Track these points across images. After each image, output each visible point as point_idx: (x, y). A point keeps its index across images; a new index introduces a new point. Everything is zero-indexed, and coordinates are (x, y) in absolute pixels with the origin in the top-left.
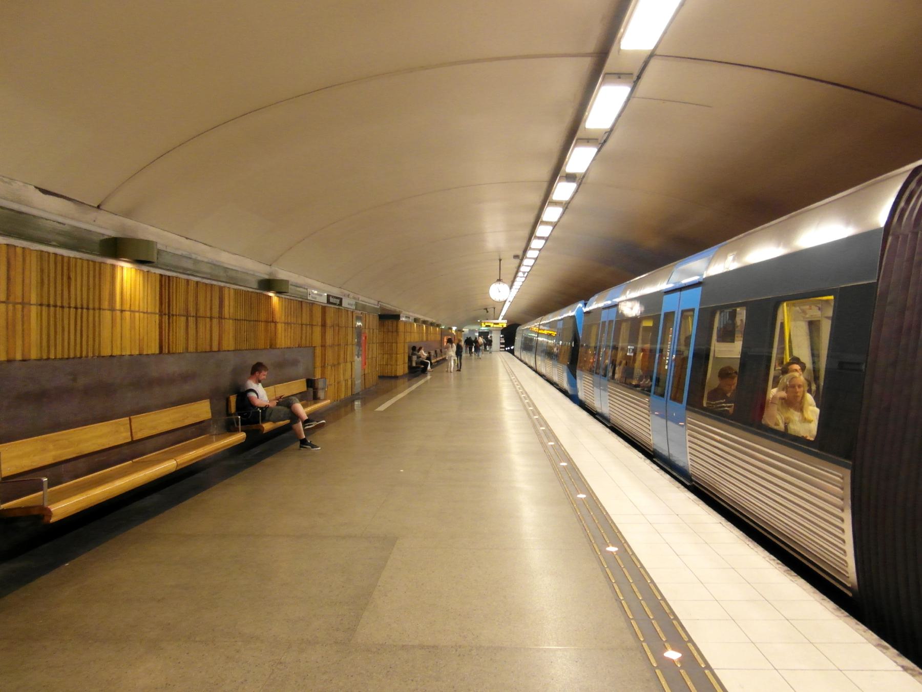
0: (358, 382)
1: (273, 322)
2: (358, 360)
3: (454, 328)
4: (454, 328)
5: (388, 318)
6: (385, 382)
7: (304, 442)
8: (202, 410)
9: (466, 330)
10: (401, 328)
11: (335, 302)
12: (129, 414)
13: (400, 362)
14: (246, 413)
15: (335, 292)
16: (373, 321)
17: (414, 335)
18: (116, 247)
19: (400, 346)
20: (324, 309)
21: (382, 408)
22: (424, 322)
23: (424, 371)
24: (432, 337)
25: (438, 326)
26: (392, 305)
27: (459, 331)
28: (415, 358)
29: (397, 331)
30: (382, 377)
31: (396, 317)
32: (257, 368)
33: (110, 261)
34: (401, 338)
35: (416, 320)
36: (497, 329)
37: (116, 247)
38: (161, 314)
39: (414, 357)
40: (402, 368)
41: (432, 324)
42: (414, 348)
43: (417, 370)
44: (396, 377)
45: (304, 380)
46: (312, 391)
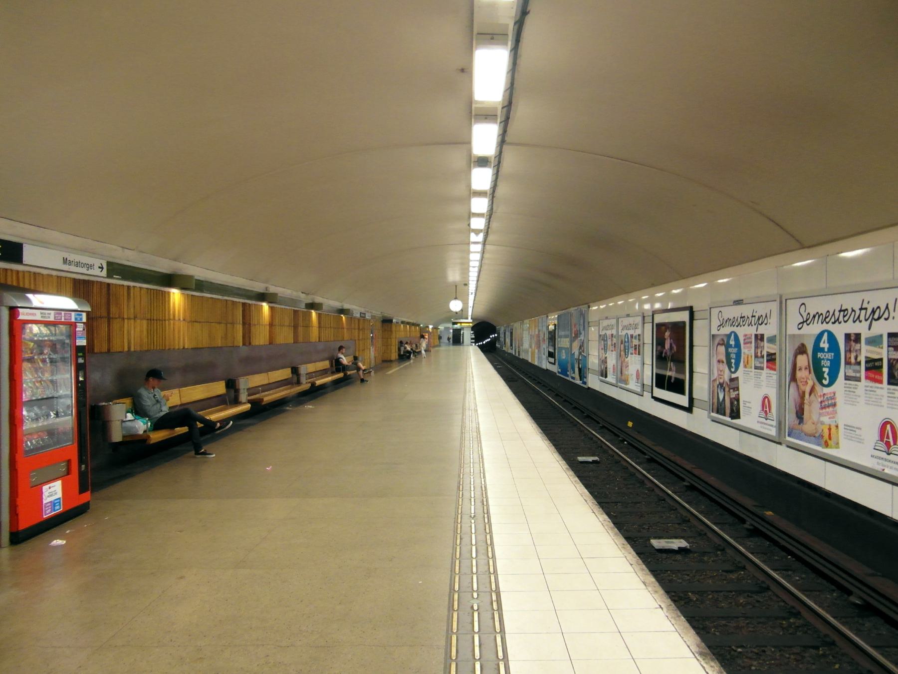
0: (373, 362)
1: (119, 317)
2: (372, 349)
3: (431, 327)
4: (431, 327)
5: (387, 321)
6: (386, 362)
7: (362, 380)
8: (326, 364)
9: (441, 327)
10: (394, 328)
11: (363, 315)
12: (267, 371)
13: (393, 351)
14: (337, 366)
15: (363, 310)
16: (379, 324)
17: (401, 333)
18: (170, 280)
19: (393, 340)
20: (359, 320)
21: (390, 372)
22: (408, 323)
23: (409, 358)
24: (413, 334)
25: (418, 325)
26: (388, 314)
27: (435, 328)
28: (402, 349)
29: (391, 331)
30: (384, 361)
31: (390, 321)
32: (341, 348)
33: (167, 289)
34: (394, 335)
35: (403, 322)
36: (467, 327)
37: (170, 280)
38: (250, 324)
39: (351, 361)
40: (394, 356)
41: (413, 324)
42: (401, 342)
43: (404, 357)
44: (391, 361)
45: (290, 369)
46: (232, 396)
